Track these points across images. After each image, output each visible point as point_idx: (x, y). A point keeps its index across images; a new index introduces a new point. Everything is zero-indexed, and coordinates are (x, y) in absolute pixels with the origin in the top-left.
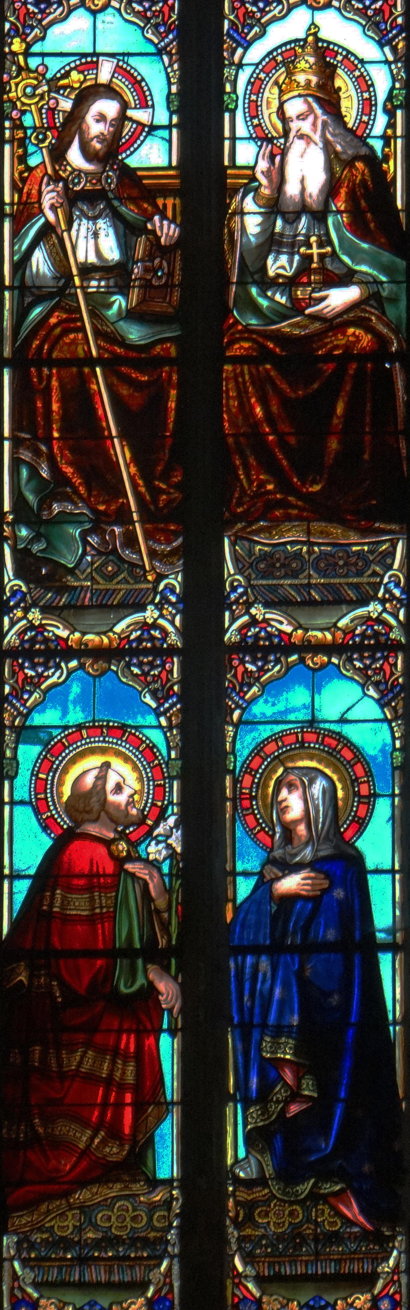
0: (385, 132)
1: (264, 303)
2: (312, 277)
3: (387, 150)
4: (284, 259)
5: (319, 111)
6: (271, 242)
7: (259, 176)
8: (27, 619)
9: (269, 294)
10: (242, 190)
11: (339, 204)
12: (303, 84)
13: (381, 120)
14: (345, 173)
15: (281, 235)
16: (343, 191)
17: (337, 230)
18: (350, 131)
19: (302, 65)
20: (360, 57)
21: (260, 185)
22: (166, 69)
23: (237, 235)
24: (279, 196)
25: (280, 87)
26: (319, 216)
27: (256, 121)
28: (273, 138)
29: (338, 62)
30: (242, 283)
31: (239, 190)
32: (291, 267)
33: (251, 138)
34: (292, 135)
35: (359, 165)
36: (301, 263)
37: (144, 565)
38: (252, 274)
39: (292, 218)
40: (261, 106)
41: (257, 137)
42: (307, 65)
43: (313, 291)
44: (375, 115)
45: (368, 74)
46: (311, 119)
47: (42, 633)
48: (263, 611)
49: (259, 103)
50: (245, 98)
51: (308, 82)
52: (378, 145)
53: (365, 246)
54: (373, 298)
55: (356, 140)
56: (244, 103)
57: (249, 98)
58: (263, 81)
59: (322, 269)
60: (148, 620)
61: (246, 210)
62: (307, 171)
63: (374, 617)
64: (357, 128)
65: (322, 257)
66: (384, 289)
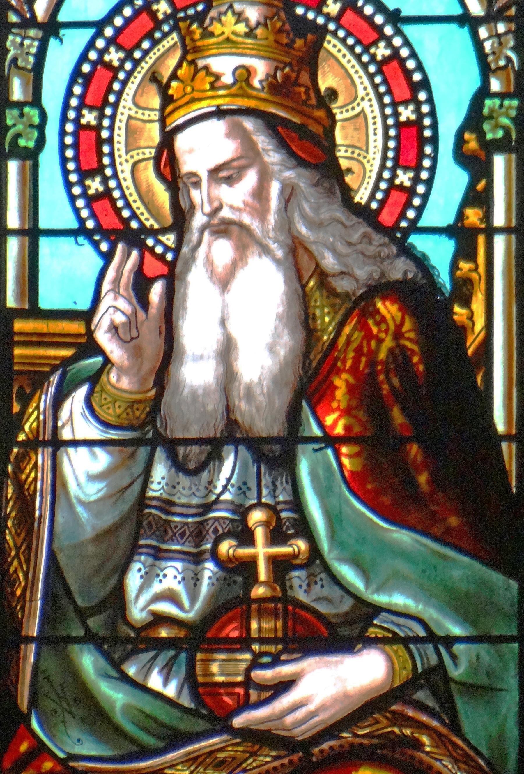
0: (461, 215)
1: (115, 696)
2: (254, 625)
3: (465, 266)
4: (172, 575)
5: (274, 157)
6: (140, 527)
7: (103, 338)
9: (131, 671)
10: (55, 379)
11: (329, 420)
12: (228, 79)
13: (450, 182)
14: (347, 330)
15: (167, 505)
16: (341, 383)
17: (324, 493)
18: (362, 212)
19: (228, 26)
20: (391, 7)
21: (107, 361)
23: (41, 505)
24: (160, 395)
25: (164, 90)
26: (275, 454)
27: (95, 185)
28: (144, 230)
29: (328, 17)
30: (53, 640)
31: (45, 377)
32: (193, 598)
33: (81, 231)
34: (198, 220)
35: (388, 309)
36: (222, 583)
38: (82, 615)
39: (196, 456)
40: (110, 141)
41: (99, 228)
42: (241, 28)
43: (255, 664)
44: (432, 169)
45: (414, 55)
46: (251, 178)
49: (105, 134)
50: (64, 119)
51: (245, 75)
52: (439, 252)
53: (403, 537)
54: (425, 685)
55: (378, 239)
56: (63, 133)
57: (76, 121)
58: (115, 71)
59: (283, 604)
61: (66, 435)
62: (238, 322)
64: (382, 203)
65: (280, 566)
66: (454, 657)
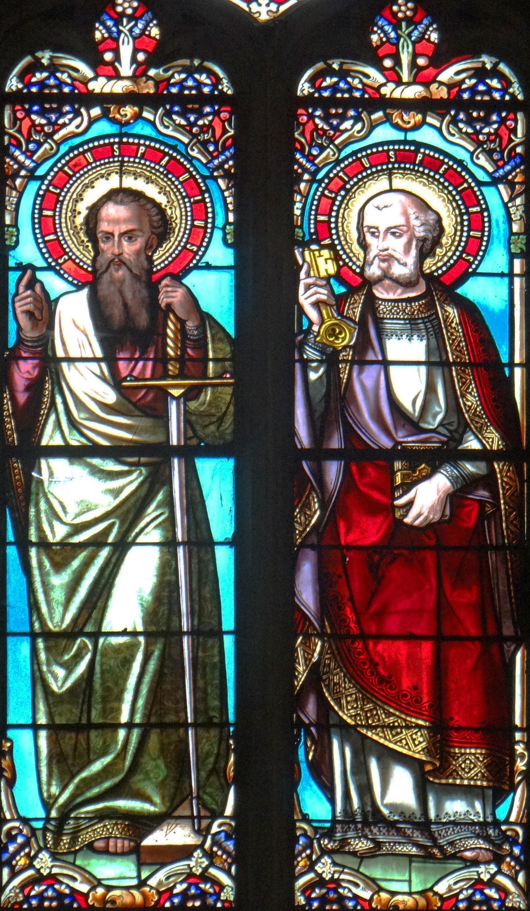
8: (316, 872)
14: (324, 312)
22: (505, 205)
37: (198, 805)
47: (335, 890)
48: (50, 865)
60: (482, 876)
63: (198, 873)
